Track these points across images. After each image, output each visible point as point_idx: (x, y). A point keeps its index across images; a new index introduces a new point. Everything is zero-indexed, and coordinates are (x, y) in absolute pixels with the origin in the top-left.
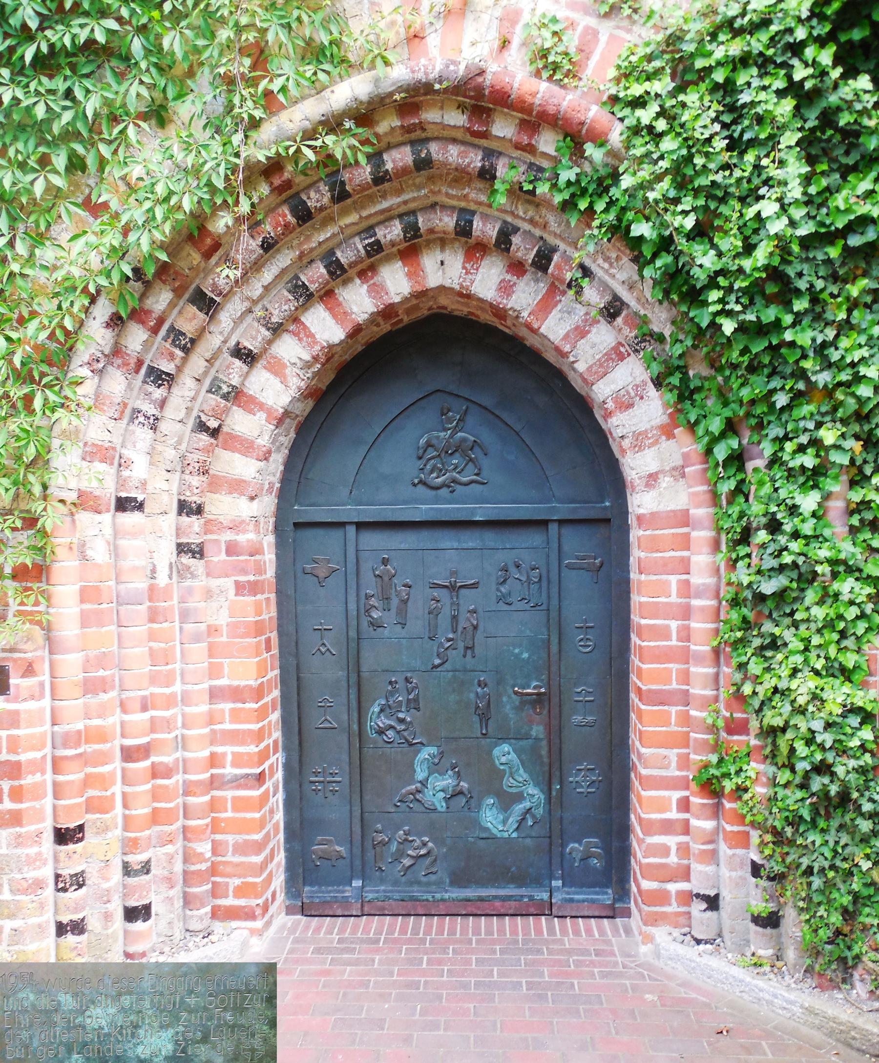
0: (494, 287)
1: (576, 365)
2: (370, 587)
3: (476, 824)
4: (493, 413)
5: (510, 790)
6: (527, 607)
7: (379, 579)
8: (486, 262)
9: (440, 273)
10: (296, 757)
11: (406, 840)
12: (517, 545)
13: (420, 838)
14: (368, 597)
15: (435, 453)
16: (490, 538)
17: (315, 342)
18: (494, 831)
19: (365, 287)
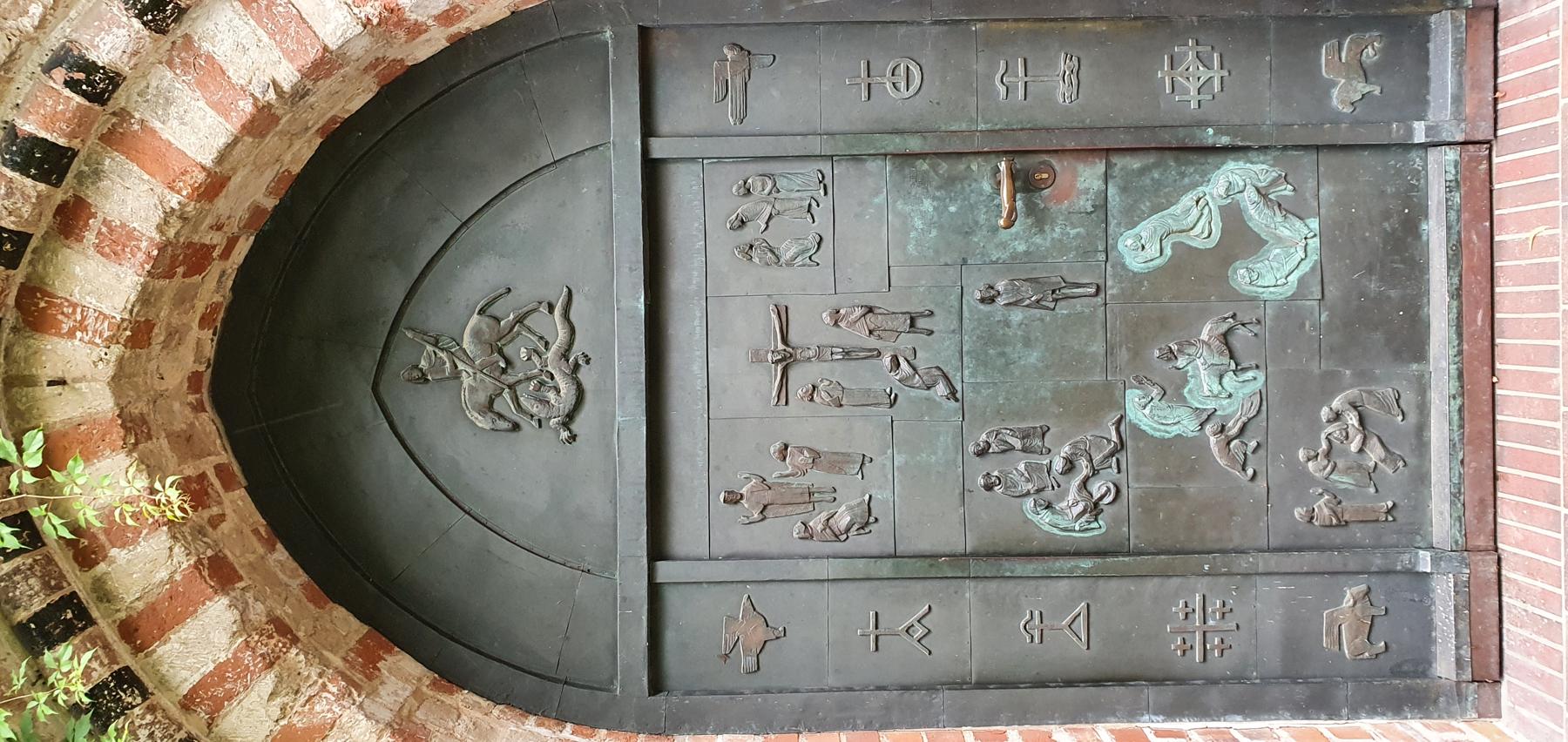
0: (114, 268)
1: (286, 87)
2: (782, 532)
3: (1289, 309)
4: (423, 274)
5: (1216, 234)
6: (826, 203)
7: (769, 513)
8: (60, 287)
9: (83, 385)
10: (1150, 693)
11: (1328, 455)
12: (698, 225)
13: (1321, 428)
14: (808, 535)
15: (506, 394)
16: (683, 279)
17: (235, 661)
18: (1305, 267)
19: (114, 552)
